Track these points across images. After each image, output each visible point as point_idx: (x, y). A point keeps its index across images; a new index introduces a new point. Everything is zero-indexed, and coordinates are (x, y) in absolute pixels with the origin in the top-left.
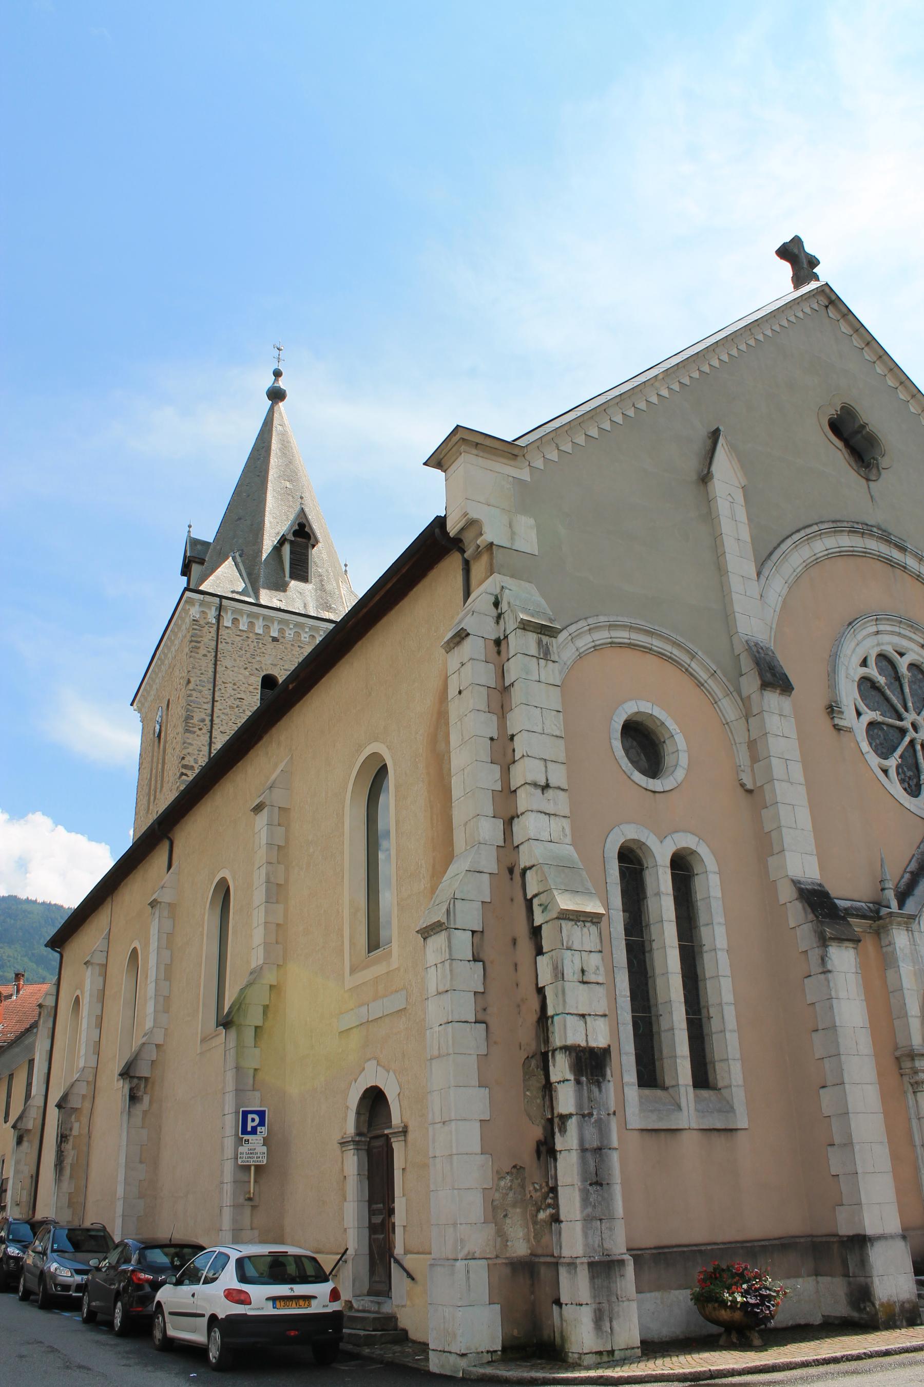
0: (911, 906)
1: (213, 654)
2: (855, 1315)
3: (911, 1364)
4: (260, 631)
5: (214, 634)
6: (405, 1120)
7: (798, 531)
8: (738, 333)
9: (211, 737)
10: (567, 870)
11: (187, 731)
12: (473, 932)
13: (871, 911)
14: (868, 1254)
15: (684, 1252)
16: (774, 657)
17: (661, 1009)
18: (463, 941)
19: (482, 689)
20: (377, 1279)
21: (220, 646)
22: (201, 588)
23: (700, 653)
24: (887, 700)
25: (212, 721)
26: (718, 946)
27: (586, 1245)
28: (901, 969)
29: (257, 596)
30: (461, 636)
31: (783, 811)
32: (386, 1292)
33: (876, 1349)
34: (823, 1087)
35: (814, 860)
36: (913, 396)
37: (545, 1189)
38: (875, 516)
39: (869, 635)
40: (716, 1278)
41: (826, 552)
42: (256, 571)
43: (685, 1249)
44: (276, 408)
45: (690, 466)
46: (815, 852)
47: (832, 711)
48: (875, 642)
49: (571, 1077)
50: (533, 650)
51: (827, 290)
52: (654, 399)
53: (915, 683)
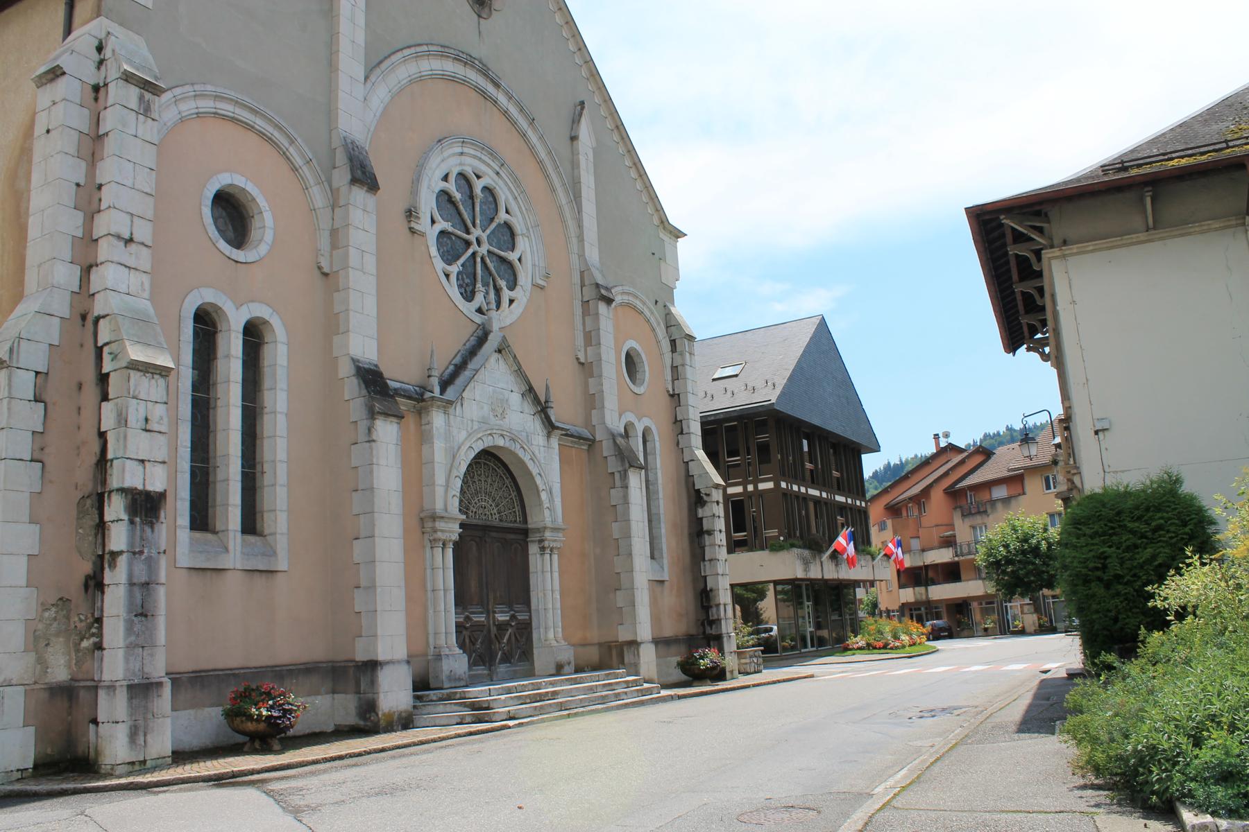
0: (450, 393)
2: (362, 723)
7: (409, 47)
10: (141, 324)
17: (219, 462)
18: (25, 383)
24: (460, 214)
26: (279, 409)
27: (127, 670)
30: (56, 73)
31: (353, 296)
35: (374, 344)
37: (90, 620)
38: (479, 51)
39: (454, 155)
47: (411, 215)
49: (126, 517)
50: (134, 104)
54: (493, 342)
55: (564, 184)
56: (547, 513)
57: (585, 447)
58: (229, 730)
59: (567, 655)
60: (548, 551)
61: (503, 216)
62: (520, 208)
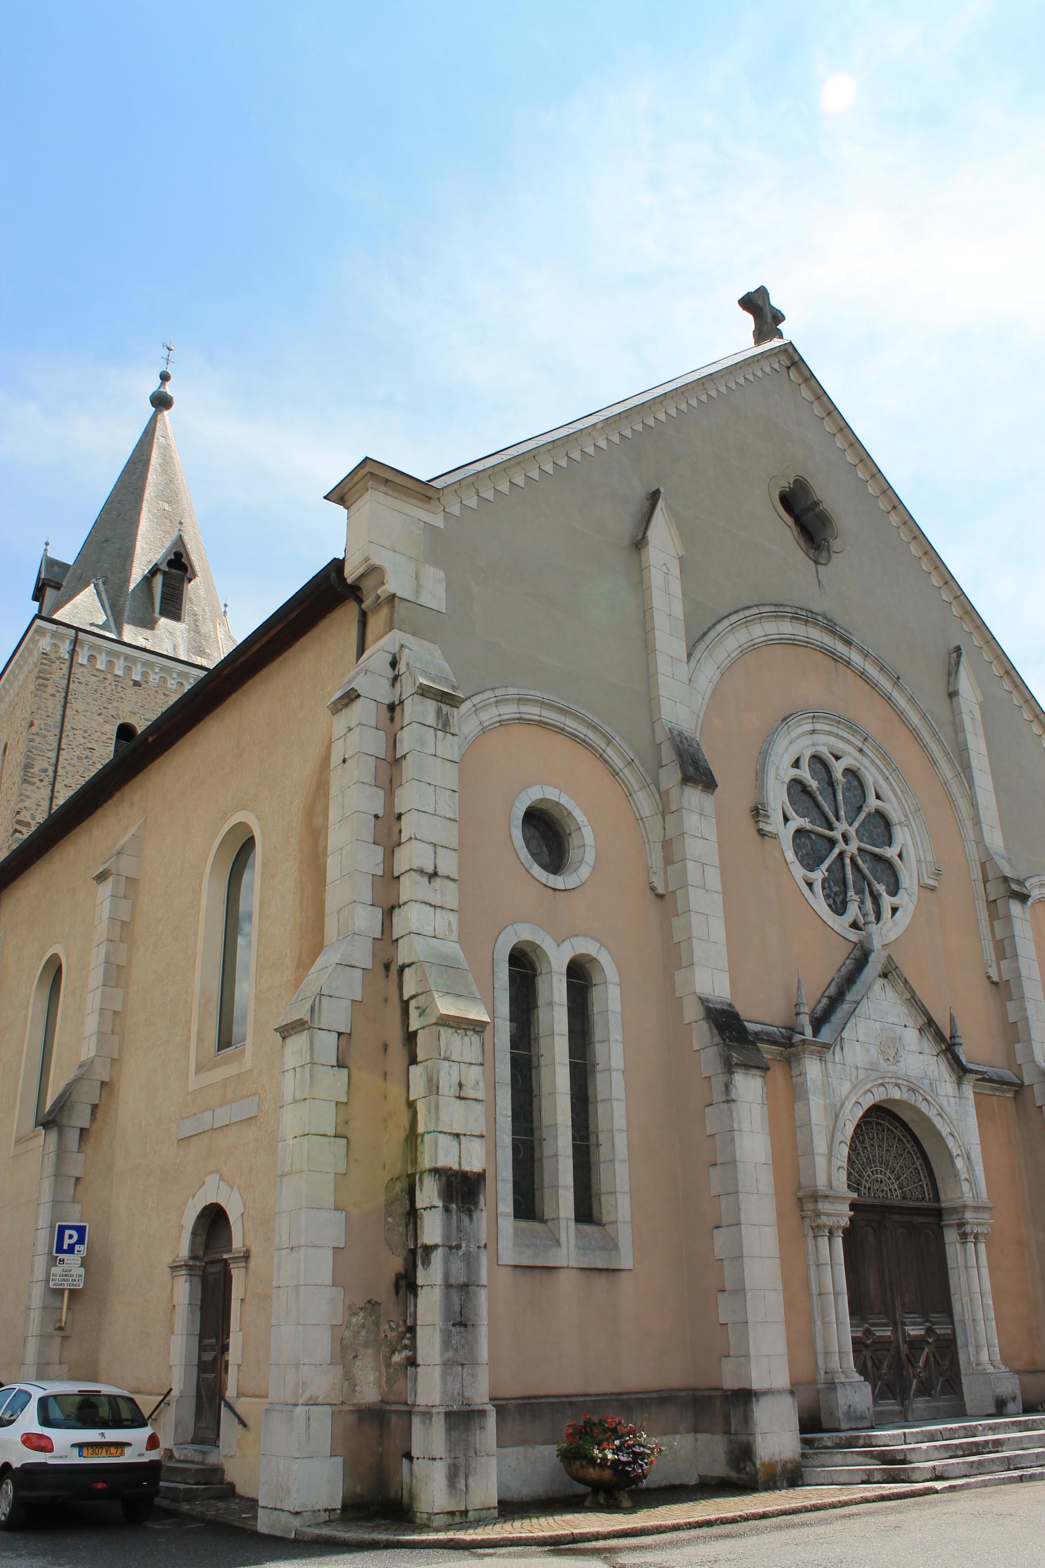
0: (826, 1034)
1: (63, 694)
2: (734, 1475)
3: (788, 1527)
4: (120, 673)
5: (65, 671)
6: (247, 1243)
7: (736, 612)
8: (690, 386)
9: (53, 791)
11: (25, 781)
12: (340, 1034)
13: (783, 1037)
14: (752, 1410)
15: (552, 1403)
16: (698, 749)
18: (327, 1042)
19: (369, 758)
20: (204, 1425)
21: (72, 686)
22: (55, 617)
23: (617, 738)
24: (818, 806)
25: (55, 771)
26: (613, 1066)
27: (444, 1393)
28: (811, 1102)
29: (120, 632)
30: (351, 697)
31: (696, 921)
32: (213, 1440)
33: (753, 1511)
34: (717, 1227)
36: (873, 476)
37: (402, 1329)
38: (821, 604)
39: (804, 734)
40: (586, 1433)
41: (765, 638)
42: (120, 603)
43: (554, 1400)
44: (159, 417)
45: (624, 527)
46: (727, 969)
48: (811, 742)
50: (431, 720)
51: (791, 350)
52: (590, 450)
53: (848, 789)
54: (875, 964)
55: (947, 754)
56: (965, 1186)
57: (1010, 1095)
58: (567, 1477)
59: (1009, 1386)
60: (971, 1238)
61: (872, 803)
62: (893, 790)
